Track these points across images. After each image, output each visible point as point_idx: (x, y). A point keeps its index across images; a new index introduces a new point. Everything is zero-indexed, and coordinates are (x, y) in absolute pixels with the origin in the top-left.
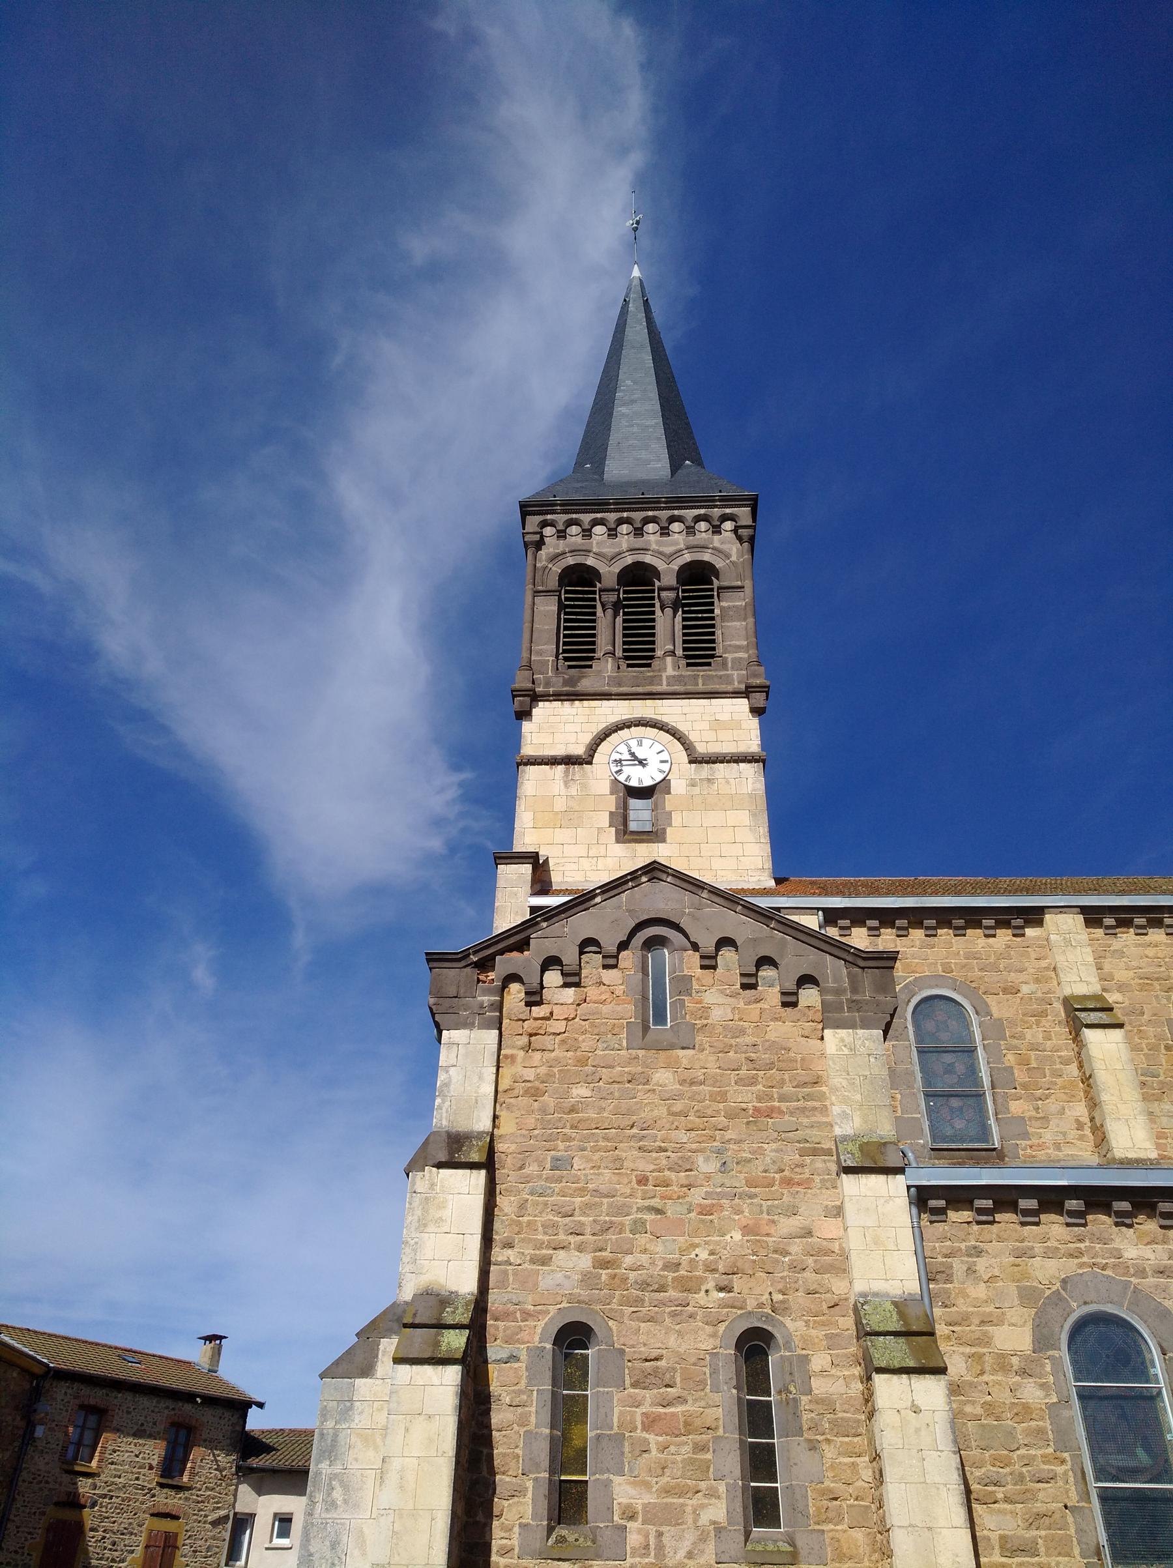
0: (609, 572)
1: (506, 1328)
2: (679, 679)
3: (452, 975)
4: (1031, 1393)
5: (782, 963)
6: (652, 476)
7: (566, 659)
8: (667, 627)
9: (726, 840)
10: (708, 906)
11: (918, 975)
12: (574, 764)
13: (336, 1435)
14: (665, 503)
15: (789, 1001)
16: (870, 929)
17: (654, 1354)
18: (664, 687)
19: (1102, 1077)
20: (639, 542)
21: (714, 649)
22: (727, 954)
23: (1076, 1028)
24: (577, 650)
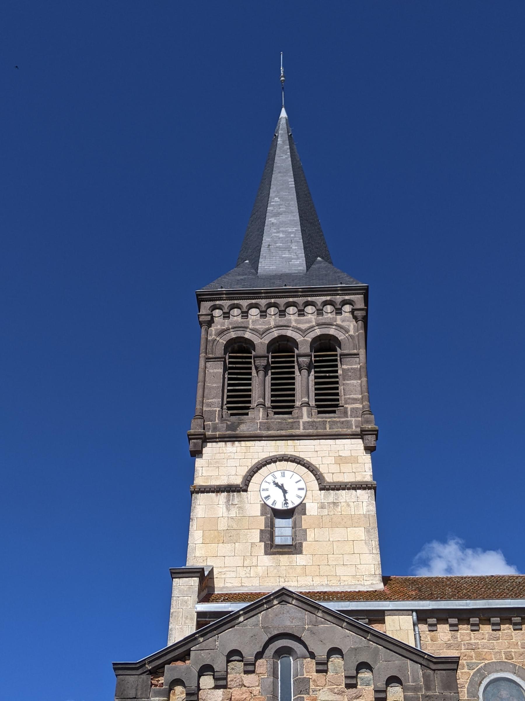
0: (261, 343)
2: (312, 424)
3: (132, 680)
5: (376, 667)
6: (293, 270)
7: (229, 409)
8: (304, 383)
9: (344, 555)
10: (322, 623)
11: (487, 662)
12: (233, 491)
14: (302, 292)
16: (451, 625)
20: (282, 321)
21: (338, 400)
22: (336, 661)
24: (238, 402)
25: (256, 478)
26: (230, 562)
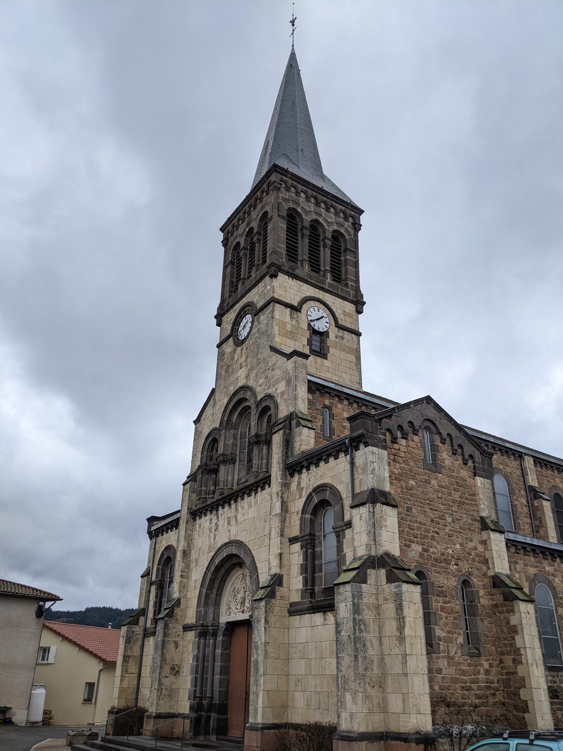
8: (325, 255)
12: (294, 310)
13: (358, 605)
17: (442, 585)
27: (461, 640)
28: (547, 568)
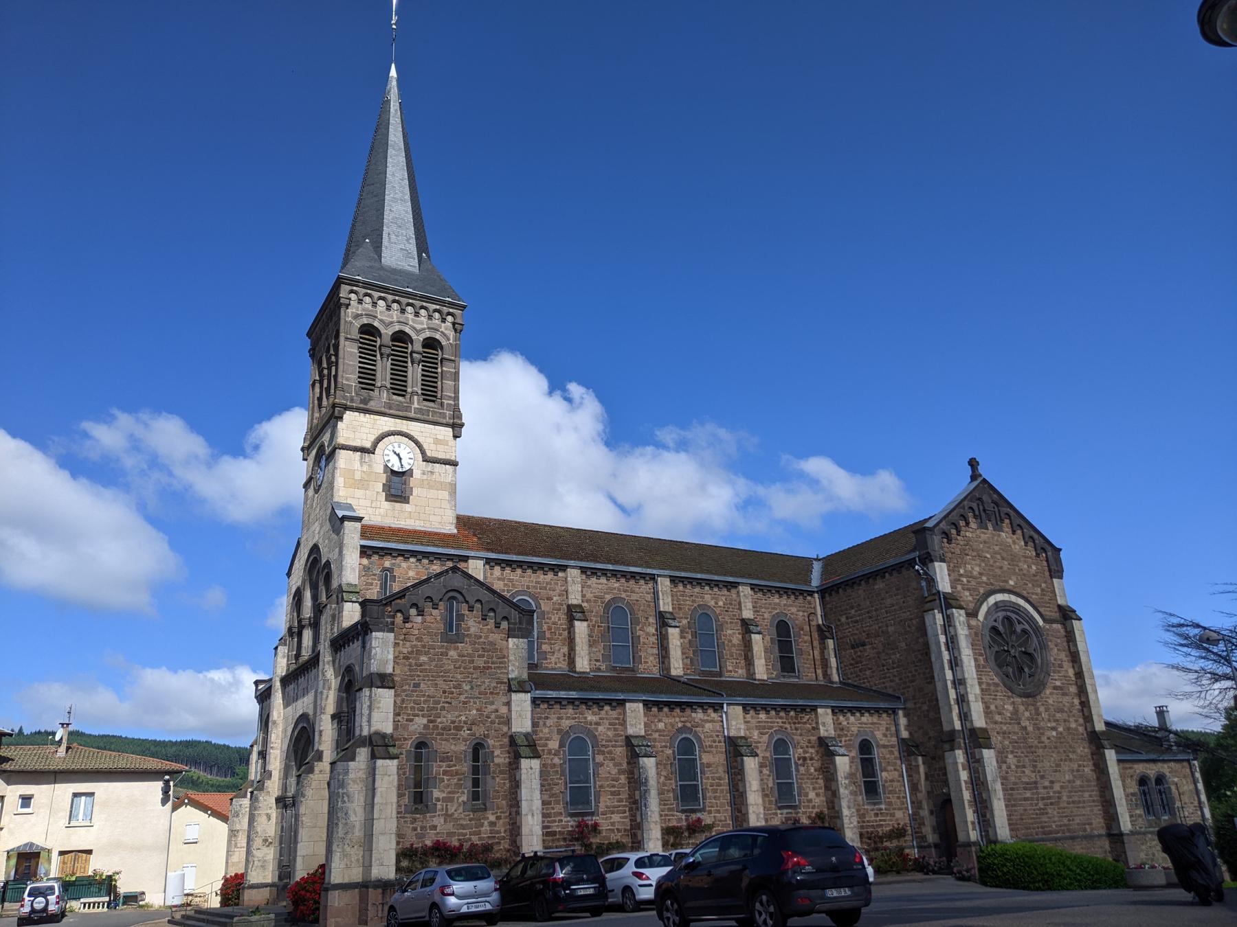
1: (798, 863)
4: (557, 760)
8: (415, 374)
15: (497, 626)
18: (412, 415)
19: (578, 640)
23: (571, 620)
24: (367, 379)
25: (381, 445)
26: (362, 502)
27: (464, 798)
28: (589, 718)
